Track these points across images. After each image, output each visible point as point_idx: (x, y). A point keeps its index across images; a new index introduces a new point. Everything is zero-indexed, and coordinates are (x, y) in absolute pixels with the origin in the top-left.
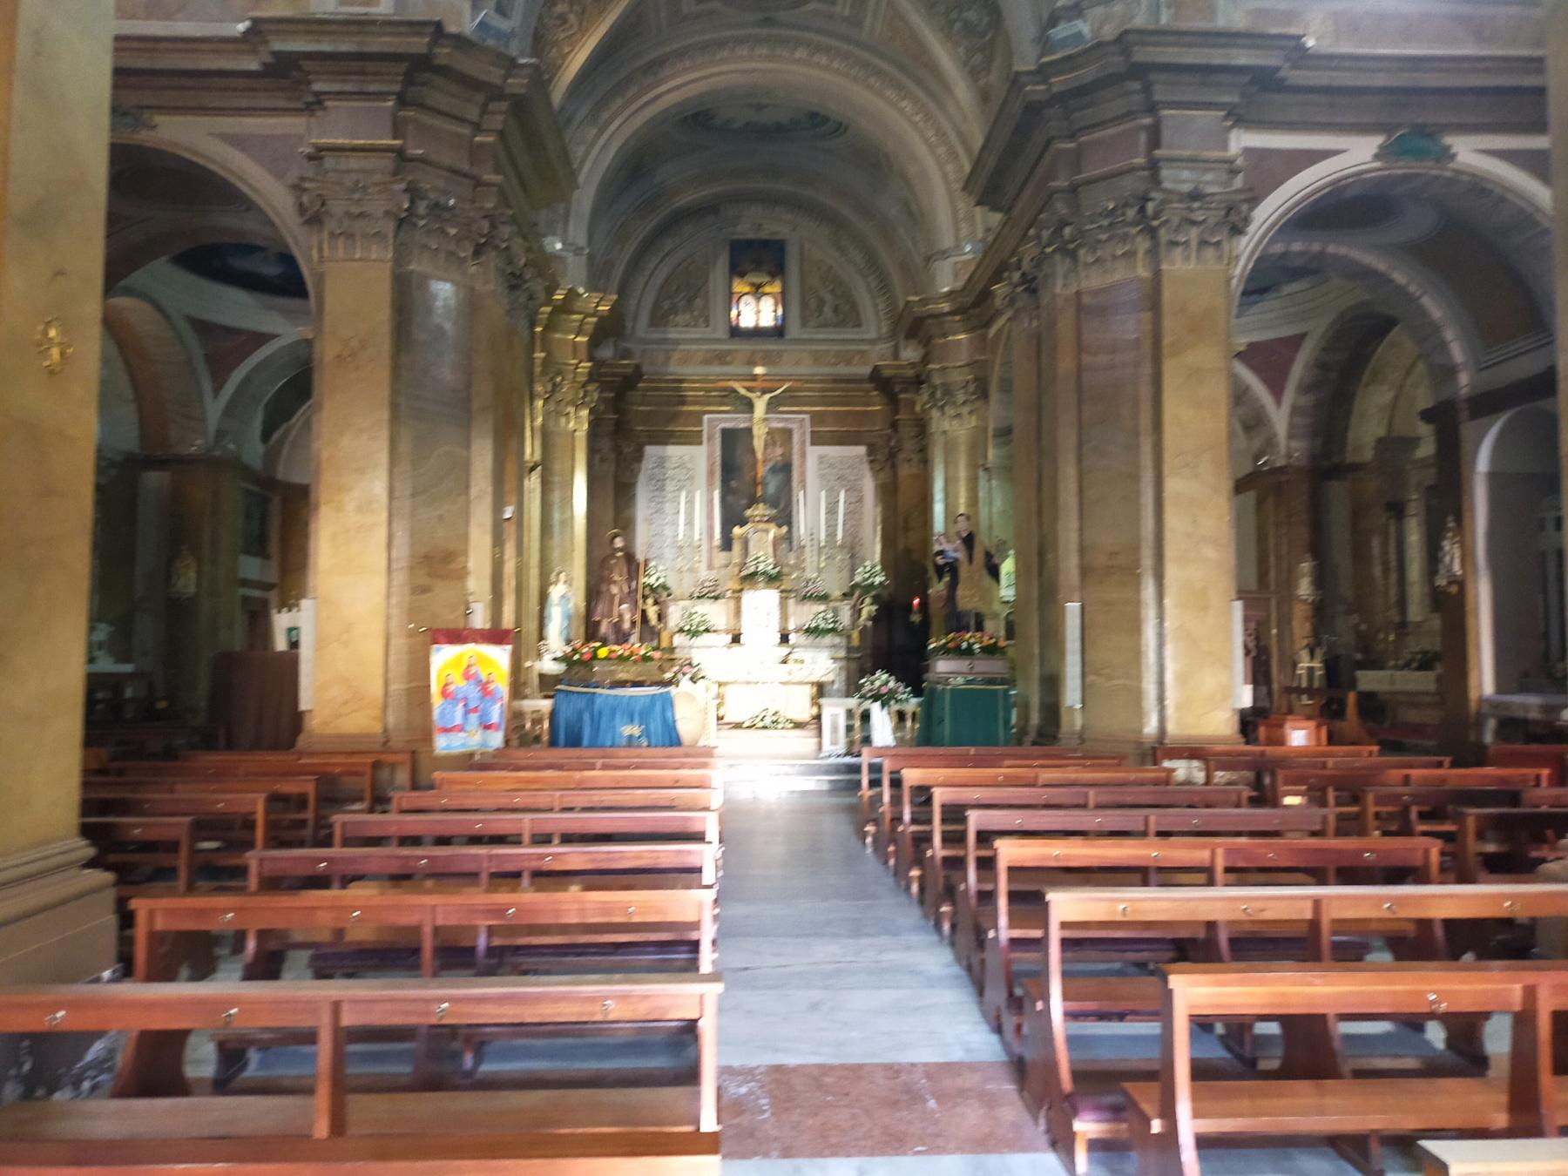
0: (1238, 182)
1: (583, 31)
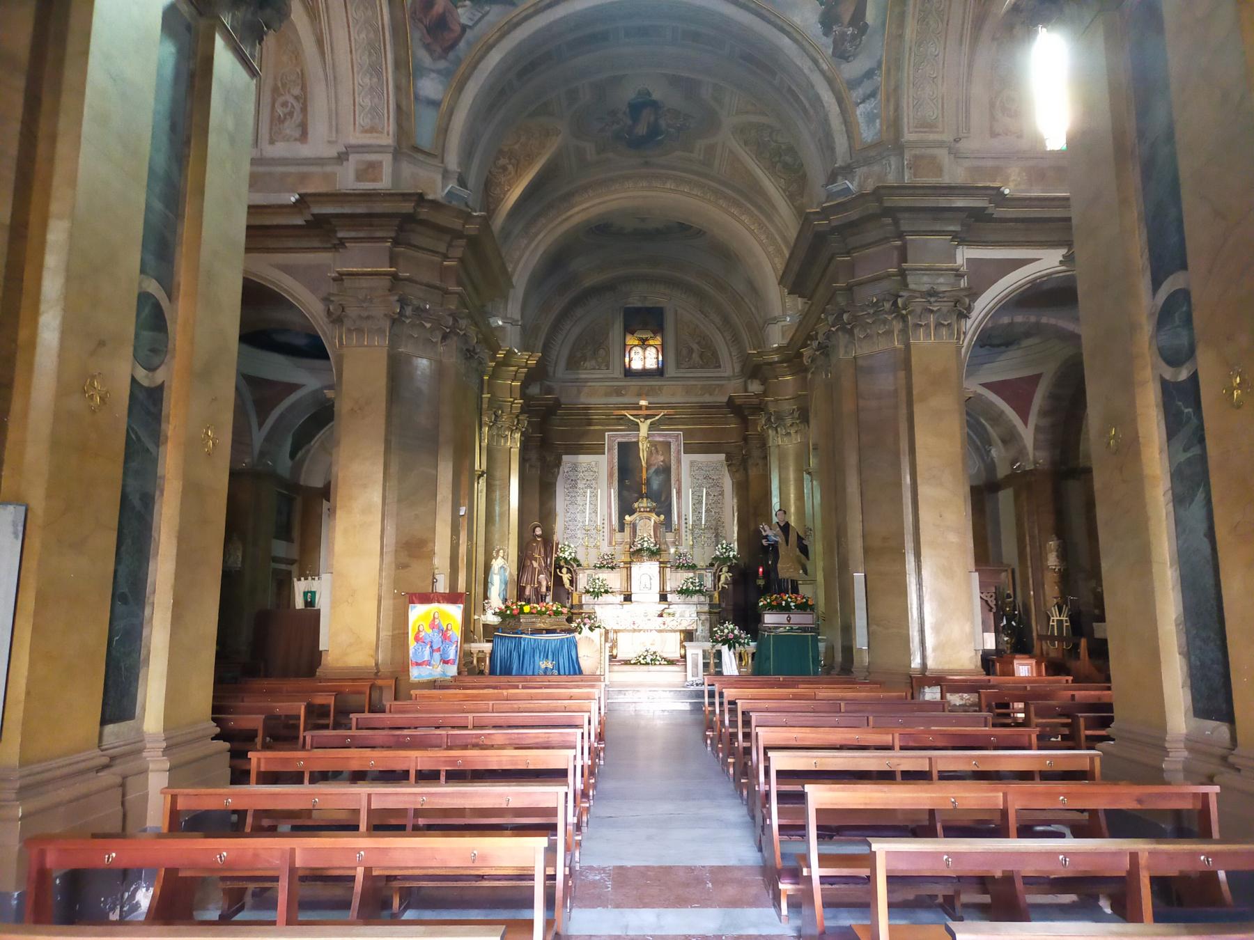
0: (963, 283)
1: (518, 175)
